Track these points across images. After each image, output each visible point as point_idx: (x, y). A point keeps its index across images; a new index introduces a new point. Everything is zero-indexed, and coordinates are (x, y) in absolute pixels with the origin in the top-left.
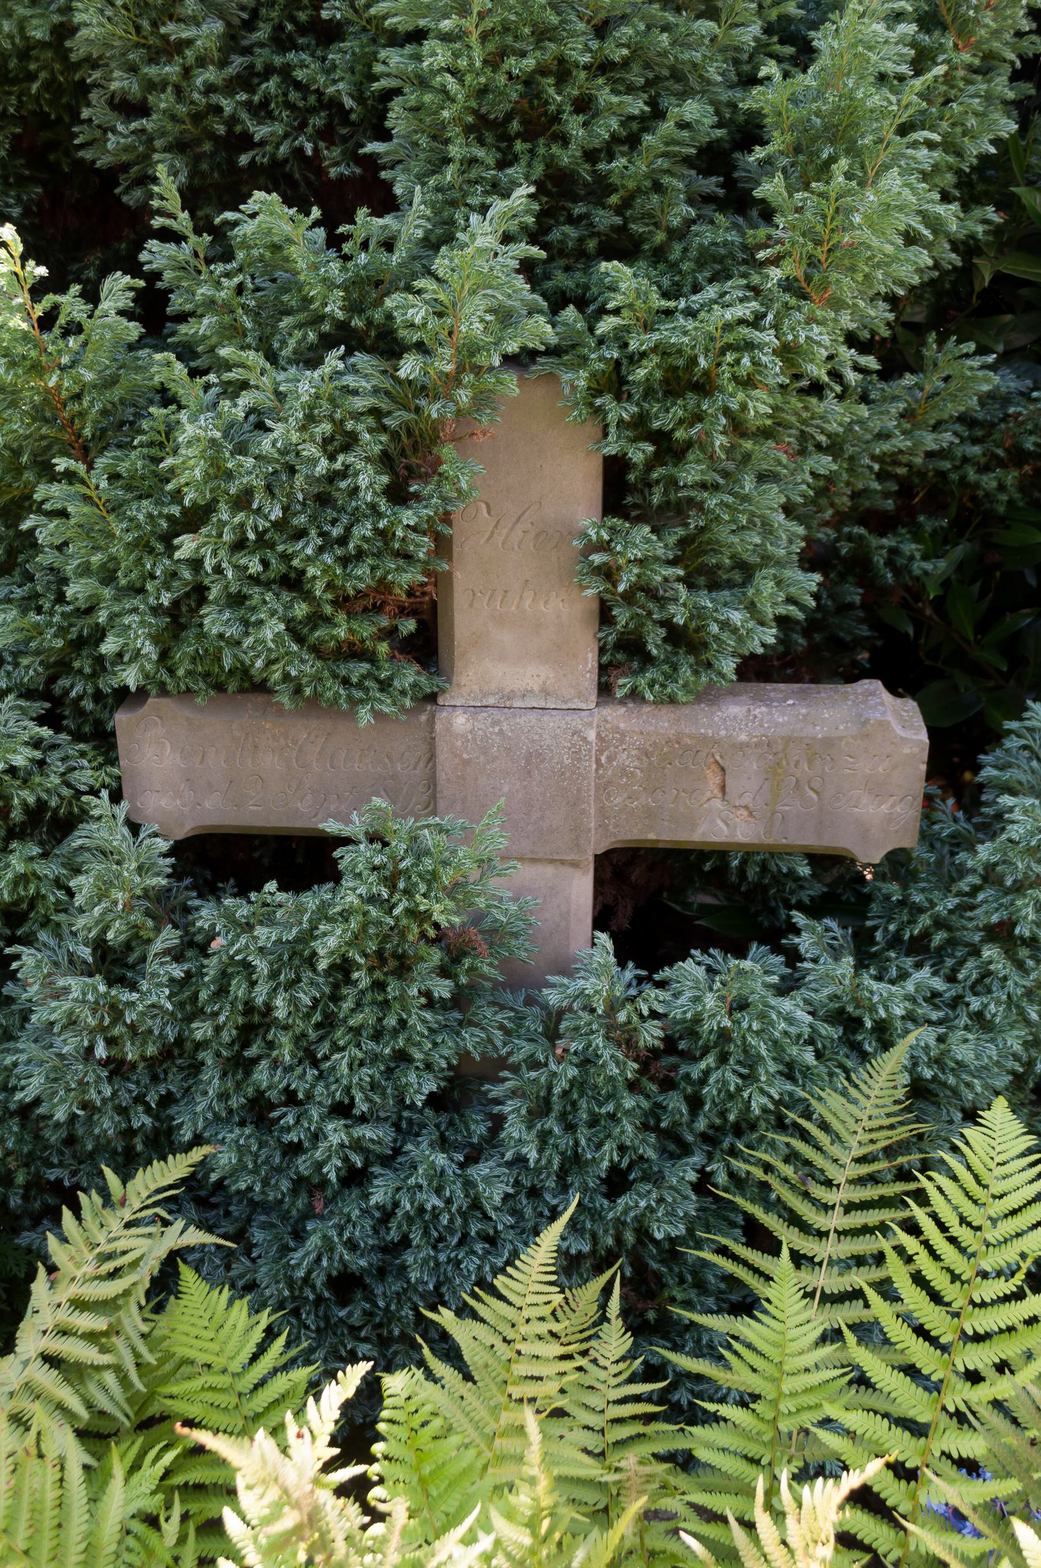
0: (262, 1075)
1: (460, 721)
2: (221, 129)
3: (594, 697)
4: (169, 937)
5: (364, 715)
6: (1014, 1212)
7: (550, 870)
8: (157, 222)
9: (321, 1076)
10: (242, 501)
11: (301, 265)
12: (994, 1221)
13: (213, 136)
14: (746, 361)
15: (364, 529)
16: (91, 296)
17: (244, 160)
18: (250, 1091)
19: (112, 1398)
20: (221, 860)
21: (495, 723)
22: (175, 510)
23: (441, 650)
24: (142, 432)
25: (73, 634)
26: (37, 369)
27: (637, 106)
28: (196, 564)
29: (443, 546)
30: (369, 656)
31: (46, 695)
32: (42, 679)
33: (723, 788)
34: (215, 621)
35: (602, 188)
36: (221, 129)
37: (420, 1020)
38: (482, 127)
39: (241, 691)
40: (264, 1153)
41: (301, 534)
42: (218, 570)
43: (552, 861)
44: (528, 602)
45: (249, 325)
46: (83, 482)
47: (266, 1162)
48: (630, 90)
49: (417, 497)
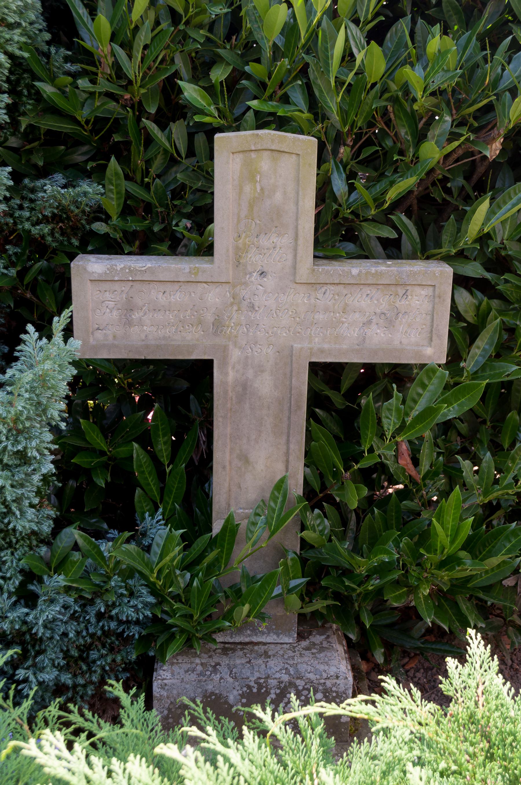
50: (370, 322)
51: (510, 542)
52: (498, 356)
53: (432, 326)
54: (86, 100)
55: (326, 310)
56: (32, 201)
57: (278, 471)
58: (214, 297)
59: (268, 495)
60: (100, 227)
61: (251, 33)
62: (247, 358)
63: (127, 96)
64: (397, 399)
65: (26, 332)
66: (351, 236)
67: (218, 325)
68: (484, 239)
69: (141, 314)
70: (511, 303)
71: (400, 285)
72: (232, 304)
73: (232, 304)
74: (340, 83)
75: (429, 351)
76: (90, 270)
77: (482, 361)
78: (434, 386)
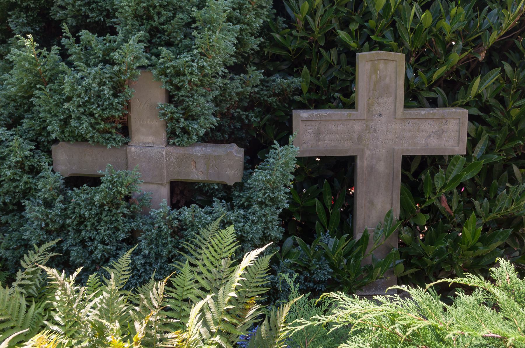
0: (83, 233)
1: (133, 149)
2: (83, 14)
3: (165, 145)
4: (61, 198)
5: (109, 146)
6: (228, 245)
7: (156, 186)
8: (64, 34)
9: (98, 234)
10: (79, 96)
11: (93, 45)
12: (225, 247)
13: (81, 15)
14: (190, 69)
15: (106, 103)
16: (49, 50)
17: (88, 21)
18: (81, 238)
19: (33, 291)
20: (74, 181)
21: (141, 150)
22: (64, 97)
23: (129, 133)
24: (57, 80)
25: (42, 126)
26: (36, 65)
27: (170, 14)
28: (69, 110)
29: (128, 108)
30: (110, 133)
31: (35, 141)
32: (35, 137)
33: (196, 167)
34: (73, 123)
35: (163, 31)
36: (83, 14)
37: (121, 219)
38: (136, 16)
39: (82, 141)
40: (84, 254)
41: (93, 104)
42: (73, 111)
43: (156, 184)
44: (148, 122)
45: (83, 57)
46: (43, 90)
47: (84, 256)
48: (170, 11)
49: (120, 96)
50: (430, 136)
51: (500, 238)
52: (487, 153)
53: (459, 137)
54: (292, 40)
55: (410, 131)
56: (267, 86)
57: (388, 208)
58: (358, 127)
59: (383, 220)
60: (297, 98)
61: (367, 7)
62: (373, 154)
63: (312, 38)
64: (442, 173)
65: (274, 144)
66: (415, 98)
67: (360, 139)
68: (479, 96)
69: (324, 135)
70: (492, 127)
71: (444, 119)
72: (366, 130)
73: (366, 130)
74: (412, 29)
75: (457, 149)
76: (301, 116)
77: (481, 154)
78: (459, 165)
